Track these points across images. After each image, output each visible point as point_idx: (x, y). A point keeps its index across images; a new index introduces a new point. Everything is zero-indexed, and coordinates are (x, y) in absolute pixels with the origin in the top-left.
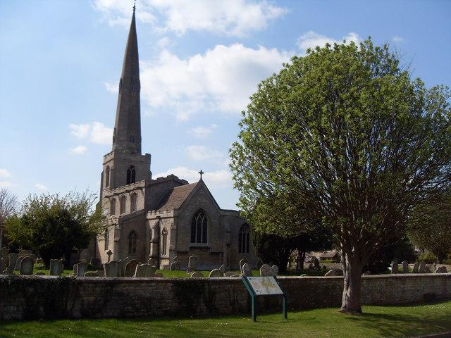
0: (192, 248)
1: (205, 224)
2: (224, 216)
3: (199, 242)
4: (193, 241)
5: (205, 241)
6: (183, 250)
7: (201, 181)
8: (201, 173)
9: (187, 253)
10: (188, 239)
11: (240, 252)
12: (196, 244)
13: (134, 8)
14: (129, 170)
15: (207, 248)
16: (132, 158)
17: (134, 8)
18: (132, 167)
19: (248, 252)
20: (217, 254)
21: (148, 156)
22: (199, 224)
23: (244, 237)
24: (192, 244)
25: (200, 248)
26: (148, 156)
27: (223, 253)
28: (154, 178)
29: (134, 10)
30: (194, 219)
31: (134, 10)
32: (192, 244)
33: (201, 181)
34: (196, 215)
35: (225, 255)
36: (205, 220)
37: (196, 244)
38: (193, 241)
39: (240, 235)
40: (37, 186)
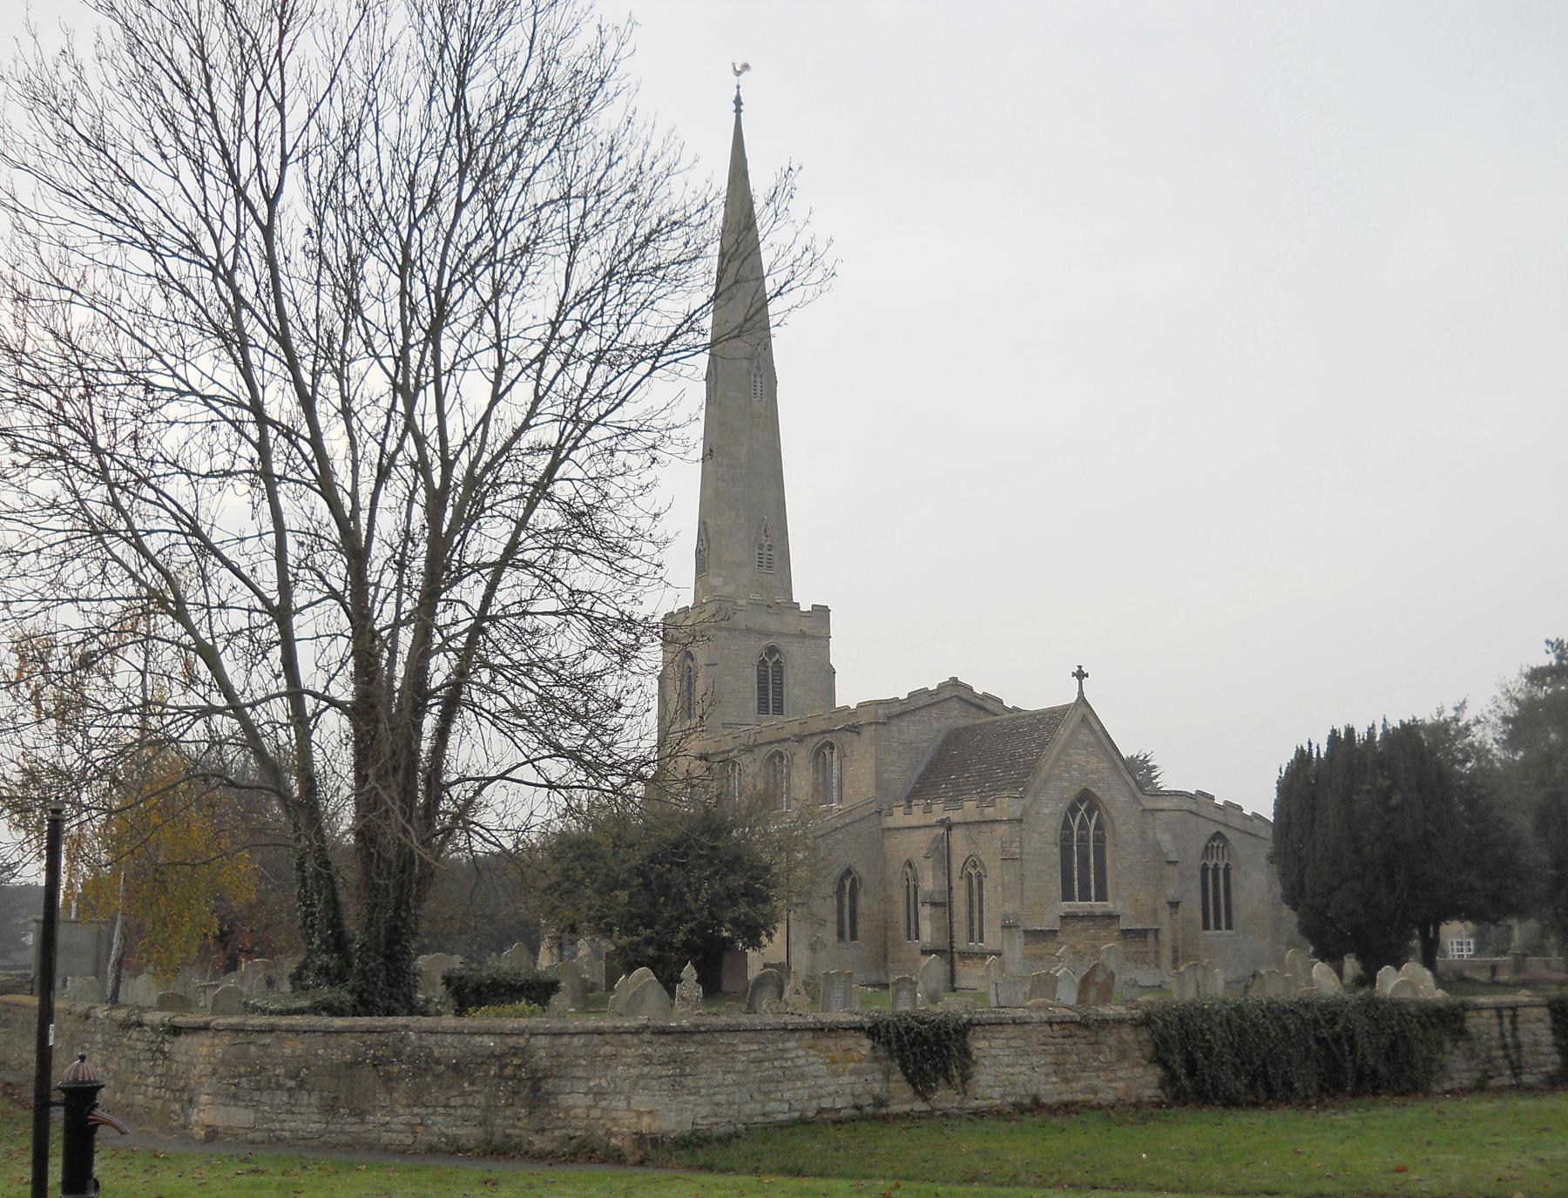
0: (1066, 918)
1: (1100, 840)
2: (1153, 810)
3: (1085, 896)
4: (1067, 895)
5: (1102, 896)
6: (1044, 926)
7: (1081, 698)
8: (1080, 675)
9: (1054, 932)
10: (1056, 889)
11: (1206, 926)
12: (1078, 906)
13: (738, 102)
14: (763, 662)
15: (1112, 917)
16: (773, 624)
17: (738, 102)
18: (772, 651)
19: (1229, 927)
20: (1142, 934)
21: (821, 613)
22: (1083, 839)
23: (1216, 878)
24: (1066, 907)
25: (1091, 917)
26: (821, 613)
27: (1156, 931)
28: (848, 694)
29: (738, 111)
30: (1066, 825)
31: (738, 111)
32: (1066, 907)
33: (1081, 698)
34: (1073, 809)
35: (1166, 937)
36: (1099, 827)
37: (1078, 906)
38: (1067, 895)
39: (1204, 869)
40: (1521, 753)
